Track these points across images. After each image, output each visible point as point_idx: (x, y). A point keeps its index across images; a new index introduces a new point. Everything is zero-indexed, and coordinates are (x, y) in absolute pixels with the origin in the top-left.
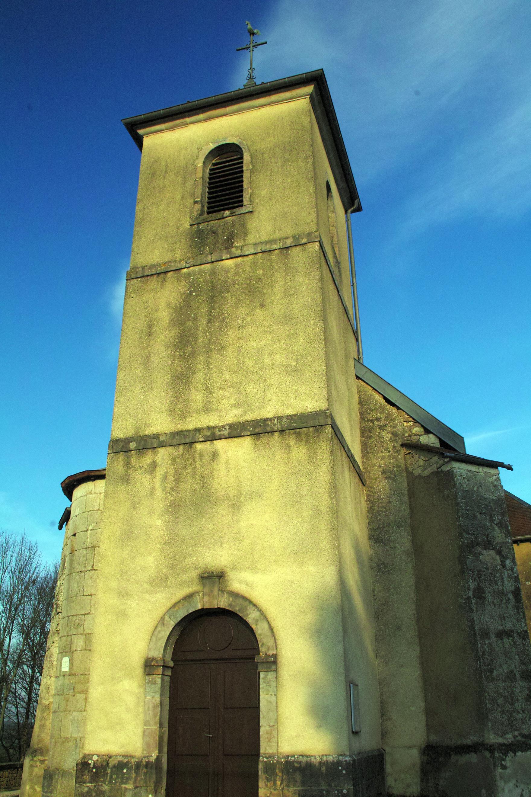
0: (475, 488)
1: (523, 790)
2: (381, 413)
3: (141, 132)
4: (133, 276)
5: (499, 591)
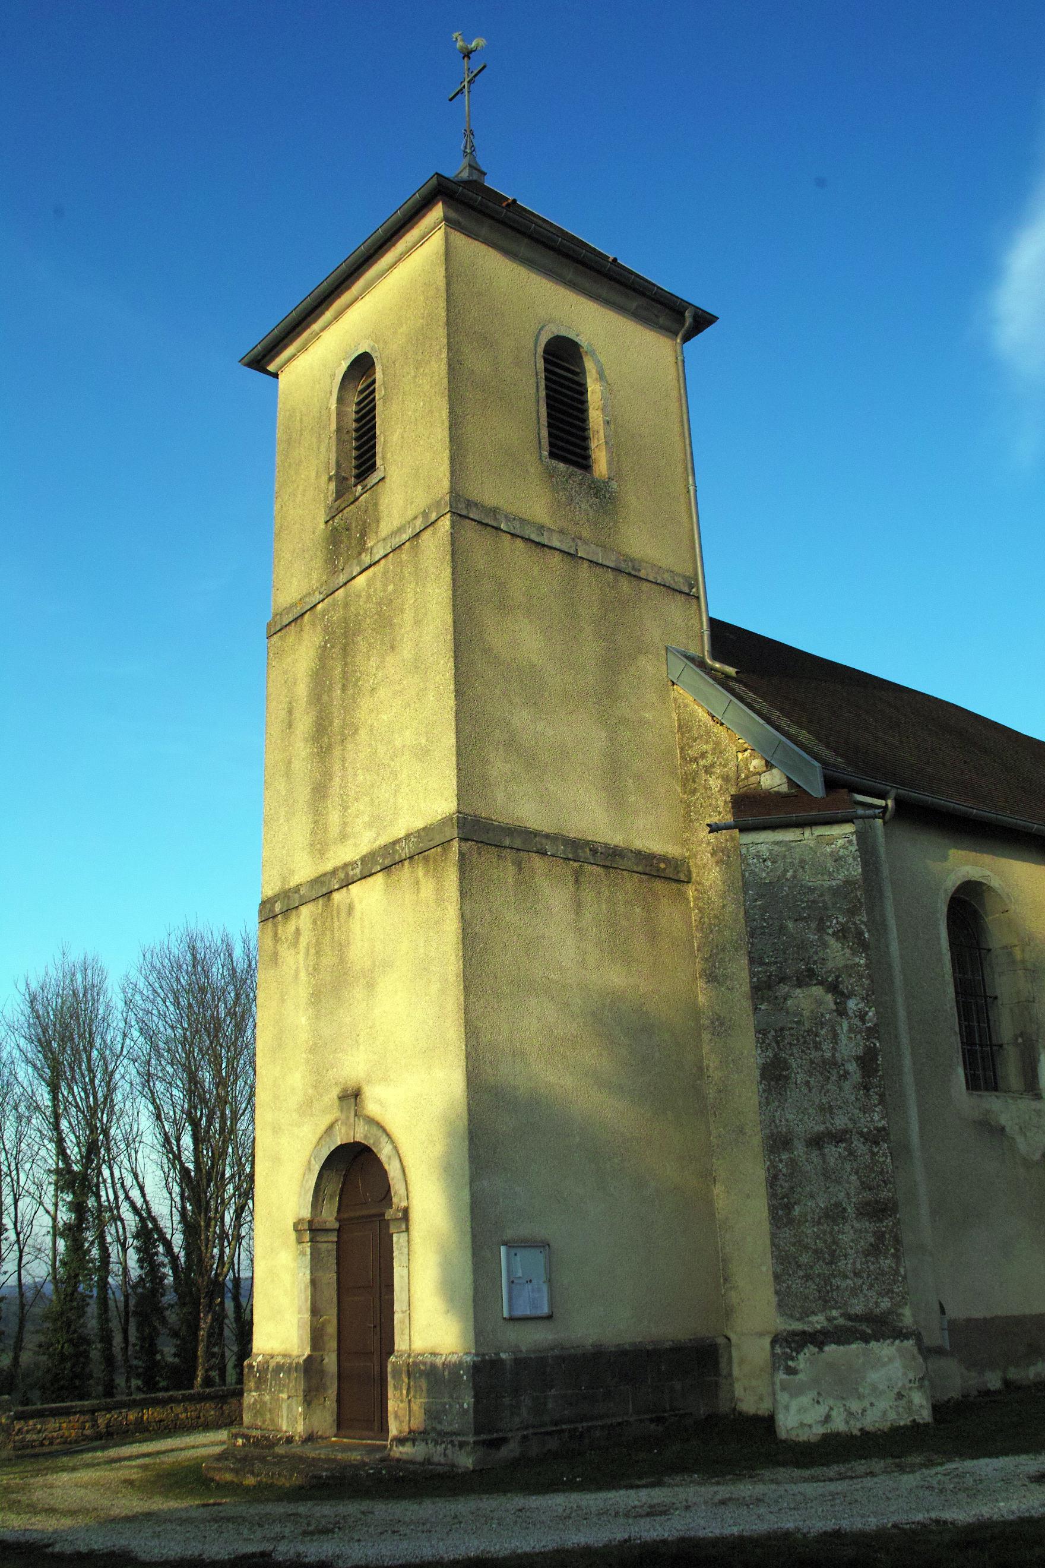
0: (789, 875)
1: (831, 1409)
2: (707, 743)
3: (271, 368)
5: (824, 1062)
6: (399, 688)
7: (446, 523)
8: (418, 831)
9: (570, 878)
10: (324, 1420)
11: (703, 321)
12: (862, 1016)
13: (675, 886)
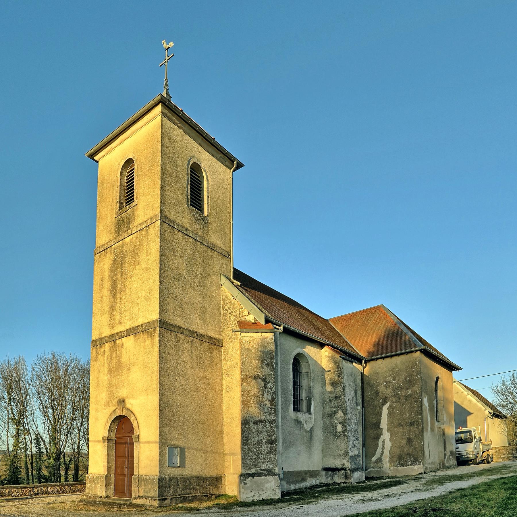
3: (96, 158)
4: (96, 253)
6: (141, 277)
7: (159, 222)
8: (146, 324)
9: (190, 342)
10: (111, 492)
11: (240, 166)
12: (271, 389)
13: (218, 347)
